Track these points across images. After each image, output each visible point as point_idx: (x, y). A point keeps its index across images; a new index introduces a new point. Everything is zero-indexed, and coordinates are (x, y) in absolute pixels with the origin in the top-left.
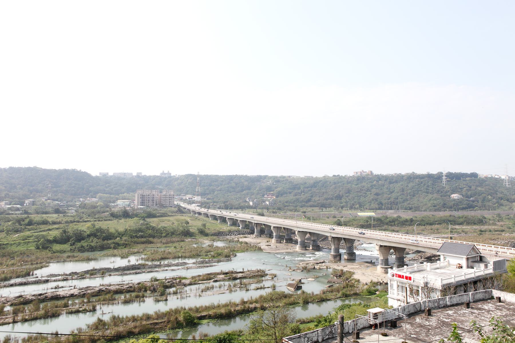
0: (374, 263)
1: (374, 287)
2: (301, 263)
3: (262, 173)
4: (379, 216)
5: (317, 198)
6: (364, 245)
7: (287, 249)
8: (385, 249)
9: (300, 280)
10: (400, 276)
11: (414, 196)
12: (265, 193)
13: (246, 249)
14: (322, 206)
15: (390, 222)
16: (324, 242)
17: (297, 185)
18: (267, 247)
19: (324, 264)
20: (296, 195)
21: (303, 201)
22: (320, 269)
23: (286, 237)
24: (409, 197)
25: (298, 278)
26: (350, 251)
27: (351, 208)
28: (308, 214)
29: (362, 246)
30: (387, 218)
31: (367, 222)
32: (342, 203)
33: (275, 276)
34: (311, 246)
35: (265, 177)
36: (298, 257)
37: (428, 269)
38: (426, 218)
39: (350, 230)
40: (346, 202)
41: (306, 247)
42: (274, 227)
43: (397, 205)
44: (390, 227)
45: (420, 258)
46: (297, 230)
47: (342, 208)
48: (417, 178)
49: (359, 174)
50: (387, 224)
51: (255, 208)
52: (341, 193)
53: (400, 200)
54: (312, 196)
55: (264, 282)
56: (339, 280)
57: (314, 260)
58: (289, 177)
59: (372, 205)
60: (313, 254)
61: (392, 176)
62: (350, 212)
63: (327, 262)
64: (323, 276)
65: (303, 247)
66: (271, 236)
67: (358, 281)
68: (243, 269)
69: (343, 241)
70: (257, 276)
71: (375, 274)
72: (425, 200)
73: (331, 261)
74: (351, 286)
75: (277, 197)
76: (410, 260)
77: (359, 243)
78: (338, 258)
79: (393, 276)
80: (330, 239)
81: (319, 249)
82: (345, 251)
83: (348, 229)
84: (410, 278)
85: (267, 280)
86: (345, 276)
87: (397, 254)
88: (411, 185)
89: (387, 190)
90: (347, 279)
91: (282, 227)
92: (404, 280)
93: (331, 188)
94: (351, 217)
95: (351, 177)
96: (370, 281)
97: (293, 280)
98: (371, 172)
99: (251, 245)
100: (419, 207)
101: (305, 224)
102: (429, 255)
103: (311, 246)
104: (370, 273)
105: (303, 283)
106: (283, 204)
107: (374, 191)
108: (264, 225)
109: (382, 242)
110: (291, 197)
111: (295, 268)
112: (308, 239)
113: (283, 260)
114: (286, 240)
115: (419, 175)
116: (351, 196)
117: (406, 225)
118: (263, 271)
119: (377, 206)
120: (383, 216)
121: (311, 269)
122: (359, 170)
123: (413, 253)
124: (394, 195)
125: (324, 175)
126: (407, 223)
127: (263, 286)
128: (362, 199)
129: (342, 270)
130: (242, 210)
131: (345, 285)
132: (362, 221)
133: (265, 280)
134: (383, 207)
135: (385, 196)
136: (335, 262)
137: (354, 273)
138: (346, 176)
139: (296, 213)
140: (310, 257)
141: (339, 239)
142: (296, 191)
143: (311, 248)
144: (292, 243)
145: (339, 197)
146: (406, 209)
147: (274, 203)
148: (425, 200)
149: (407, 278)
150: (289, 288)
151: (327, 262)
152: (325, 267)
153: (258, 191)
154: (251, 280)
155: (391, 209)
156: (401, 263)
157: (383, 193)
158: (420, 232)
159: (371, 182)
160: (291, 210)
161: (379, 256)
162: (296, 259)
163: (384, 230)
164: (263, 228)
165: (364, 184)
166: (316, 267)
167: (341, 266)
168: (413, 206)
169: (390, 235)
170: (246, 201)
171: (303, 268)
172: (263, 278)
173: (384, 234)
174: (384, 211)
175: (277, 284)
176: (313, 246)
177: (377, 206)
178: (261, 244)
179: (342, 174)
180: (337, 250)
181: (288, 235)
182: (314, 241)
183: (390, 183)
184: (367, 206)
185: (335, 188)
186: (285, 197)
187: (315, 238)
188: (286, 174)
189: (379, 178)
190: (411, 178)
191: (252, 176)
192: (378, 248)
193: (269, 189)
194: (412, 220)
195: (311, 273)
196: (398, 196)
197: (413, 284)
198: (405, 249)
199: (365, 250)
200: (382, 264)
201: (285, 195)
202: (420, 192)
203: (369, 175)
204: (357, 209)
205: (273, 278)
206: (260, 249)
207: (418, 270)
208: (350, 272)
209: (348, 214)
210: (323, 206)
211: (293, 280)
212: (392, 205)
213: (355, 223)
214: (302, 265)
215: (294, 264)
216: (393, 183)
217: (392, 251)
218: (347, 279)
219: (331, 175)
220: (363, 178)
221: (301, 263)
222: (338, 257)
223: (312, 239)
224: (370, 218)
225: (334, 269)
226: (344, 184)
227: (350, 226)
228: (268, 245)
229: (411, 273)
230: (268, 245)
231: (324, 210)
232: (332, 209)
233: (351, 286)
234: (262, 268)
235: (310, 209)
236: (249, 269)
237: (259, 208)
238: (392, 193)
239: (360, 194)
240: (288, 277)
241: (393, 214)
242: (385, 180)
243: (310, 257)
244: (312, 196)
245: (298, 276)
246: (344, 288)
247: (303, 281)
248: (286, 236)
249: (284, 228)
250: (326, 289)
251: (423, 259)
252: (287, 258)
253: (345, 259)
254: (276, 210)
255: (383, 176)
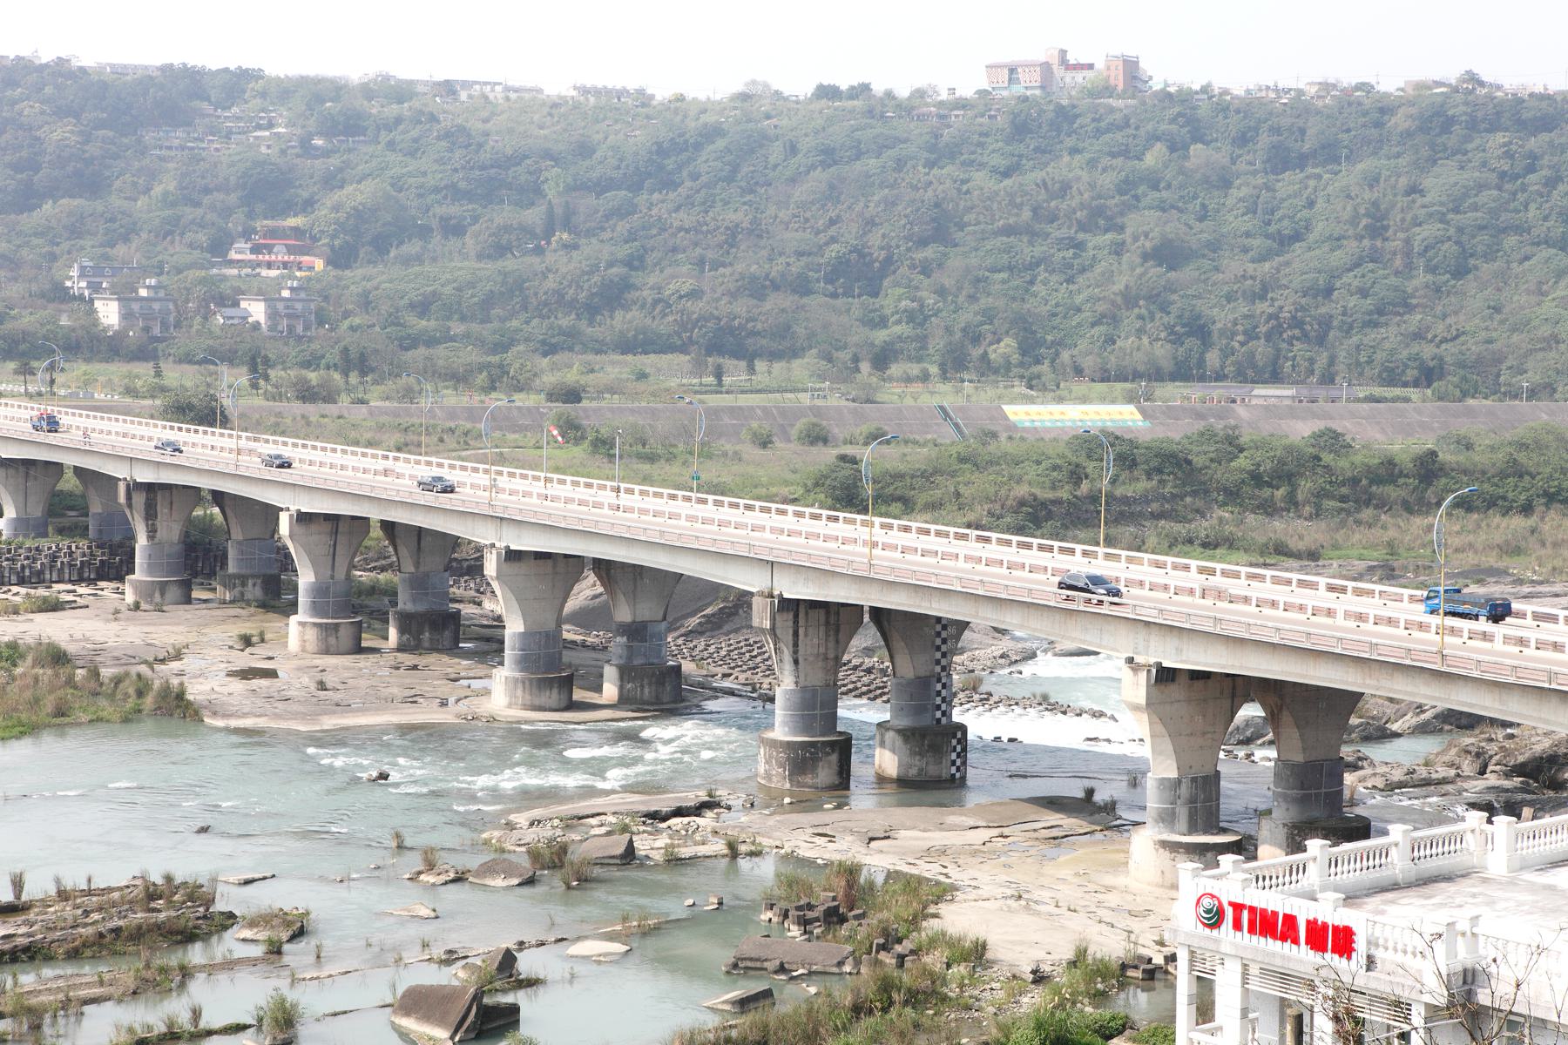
0: (1110, 807)
1: (1100, 997)
2: (521, 819)
3: (212, 50)
4: (1175, 432)
5: (679, 279)
6: (1046, 667)
7: (412, 700)
8: (1197, 698)
9: (508, 959)
10: (1267, 924)
11: (1460, 272)
12: (235, 223)
13: (49, 704)
14: (715, 348)
15: (1256, 478)
16: (722, 644)
17: (516, 159)
18: (238, 686)
19: (706, 821)
20: (501, 250)
21: (559, 301)
22: (674, 861)
23: (405, 603)
24: (1421, 278)
25: (485, 943)
26: (919, 710)
27: (955, 364)
28: (596, 412)
29: (1028, 669)
30: (1232, 445)
31: (1077, 475)
32: (883, 323)
33: (299, 934)
34: (610, 672)
35: (238, 83)
36: (501, 760)
37: (1497, 864)
38: (1540, 446)
39: (931, 542)
40: (917, 317)
41: (567, 683)
42: (303, 518)
43: (1321, 340)
44: (1251, 518)
45: (1468, 767)
46: (492, 540)
47: (882, 359)
48: (1494, 128)
49: (1029, 83)
50: (1232, 495)
51: (144, 353)
52: (875, 239)
53: (1345, 301)
54: (635, 263)
55: (199, 989)
56: (825, 951)
57: (627, 789)
58: (448, 88)
59: (1126, 343)
60: (632, 737)
61: (1300, 107)
62: (945, 395)
63: (737, 802)
64: (694, 920)
65: (544, 684)
66: (275, 594)
67: (977, 954)
68: (18, 884)
69: (867, 636)
70: (137, 935)
71: (1112, 899)
72: (1548, 308)
73: (772, 800)
74: (915, 998)
75: (340, 259)
76: (1391, 787)
77: (1005, 644)
78: (825, 773)
79: (1214, 919)
80: (761, 616)
81: (679, 696)
82: (887, 716)
83: (910, 539)
84: (1343, 941)
85: (230, 965)
86: (874, 920)
87: (1292, 734)
88: (1441, 181)
89: (1247, 223)
90: (890, 939)
91: (375, 514)
92: (1300, 957)
93: (799, 193)
94: (947, 434)
95: (962, 104)
96: (1069, 955)
97: (450, 958)
98: (1131, 67)
99: (95, 673)
100: (1498, 359)
101: (566, 491)
102: (1541, 746)
103: (610, 672)
104: (1068, 893)
105: (531, 983)
106: (393, 320)
107: (1145, 225)
108: (218, 497)
109: (1172, 642)
110: (458, 266)
111: (473, 862)
112: (584, 618)
113: (378, 794)
114: (408, 623)
115: (1518, 102)
116: (955, 262)
117: (1383, 505)
118: (198, 895)
119: (1163, 352)
120: (1208, 435)
121: (601, 863)
122: (1032, 48)
123: (1423, 729)
124: (1302, 263)
125: (738, 87)
126: (1391, 492)
127: (184, 1020)
128: (1047, 294)
129: (851, 872)
130: (26, 371)
131: (869, 991)
132: (1031, 471)
133: (211, 969)
134: (1213, 358)
135: (1234, 265)
136: (803, 804)
137: (944, 892)
138: (920, 94)
139: (497, 400)
140: (598, 767)
141: (835, 620)
142: (504, 214)
143: (610, 691)
144: (453, 649)
145: (859, 274)
146: (1391, 377)
147: (308, 316)
148: (1548, 308)
149: (1318, 936)
150: (409, 1023)
151: (737, 802)
152: (719, 847)
153: (168, 201)
154: (88, 971)
155: (1275, 378)
156: (1323, 809)
157: (1214, 246)
158: (1491, 560)
159: (1125, 152)
160: (459, 379)
161: (1145, 751)
162: (484, 781)
163: (1209, 545)
164: (206, 526)
165: (1066, 167)
166: (642, 845)
167: (878, 839)
168: (1449, 351)
169: (1237, 587)
170: (60, 295)
171: (534, 855)
172: (196, 954)
173: (1194, 579)
174: (1218, 391)
175: (310, 1000)
176: (625, 673)
177: (1163, 352)
178: (189, 663)
179: (895, 76)
180: (818, 706)
181: (419, 583)
182: (636, 632)
183: (1281, 161)
184: (1084, 349)
185: (832, 193)
186: (407, 261)
187: (647, 610)
188: (418, 61)
189: (1192, 117)
190: (1448, 124)
191: (119, 71)
192: (1137, 688)
193: (269, 191)
194: (1428, 469)
195: (600, 893)
196: (1334, 275)
197: (1363, 980)
198: (1356, 697)
199: (1047, 703)
200: (1167, 818)
201: (412, 247)
202: (1511, 241)
203: (1108, 90)
204: (1002, 371)
205: (275, 950)
206: (177, 708)
207: (1412, 876)
208: (911, 884)
209: (924, 408)
210: (727, 344)
211: (450, 958)
212: (1287, 345)
213: (977, 484)
214: (529, 831)
215: (465, 822)
216: (1302, 161)
217: (1251, 711)
218: (890, 939)
219: (798, 84)
220: (1065, 116)
221: (521, 819)
222: (824, 761)
223: (624, 614)
224: (1091, 444)
225: (791, 858)
226: (900, 164)
227: (934, 506)
228: (246, 674)
229: (1352, 898)
230: (246, 674)
231: (736, 374)
232: (800, 369)
233: (915, 998)
234: (188, 862)
235: (616, 368)
236: (75, 879)
237: (175, 355)
238: (1285, 241)
239: (1028, 251)
240: (415, 931)
241: (1292, 413)
242: (1243, 140)
243: (598, 767)
244: (635, 263)
245: (488, 923)
246: (858, 1010)
247: (527, 964)
248: (408, 593)
249: (389, 527)
250: (712, 1021)
251: (1492, 780)
252: (409, 771)
253: (882, 780)
254: (325, 368)
255: (1223, 105)
